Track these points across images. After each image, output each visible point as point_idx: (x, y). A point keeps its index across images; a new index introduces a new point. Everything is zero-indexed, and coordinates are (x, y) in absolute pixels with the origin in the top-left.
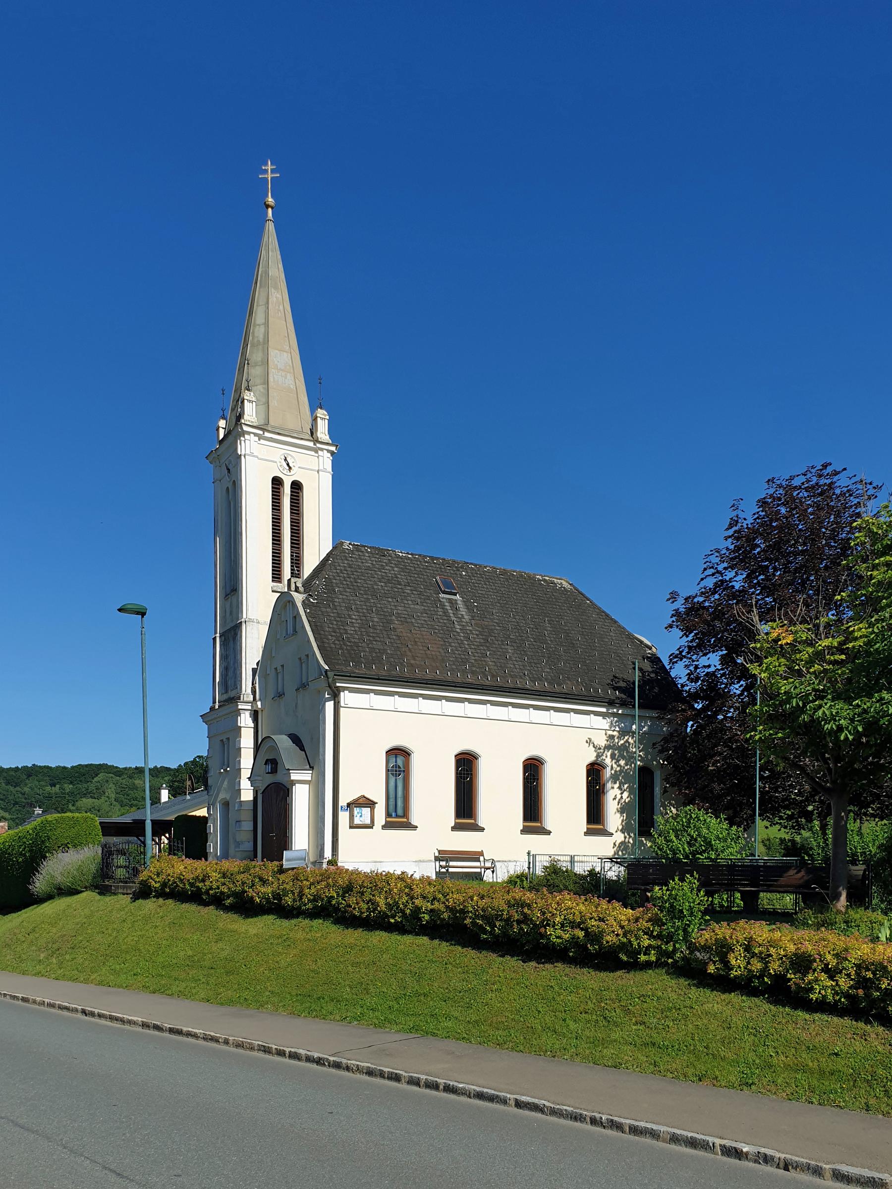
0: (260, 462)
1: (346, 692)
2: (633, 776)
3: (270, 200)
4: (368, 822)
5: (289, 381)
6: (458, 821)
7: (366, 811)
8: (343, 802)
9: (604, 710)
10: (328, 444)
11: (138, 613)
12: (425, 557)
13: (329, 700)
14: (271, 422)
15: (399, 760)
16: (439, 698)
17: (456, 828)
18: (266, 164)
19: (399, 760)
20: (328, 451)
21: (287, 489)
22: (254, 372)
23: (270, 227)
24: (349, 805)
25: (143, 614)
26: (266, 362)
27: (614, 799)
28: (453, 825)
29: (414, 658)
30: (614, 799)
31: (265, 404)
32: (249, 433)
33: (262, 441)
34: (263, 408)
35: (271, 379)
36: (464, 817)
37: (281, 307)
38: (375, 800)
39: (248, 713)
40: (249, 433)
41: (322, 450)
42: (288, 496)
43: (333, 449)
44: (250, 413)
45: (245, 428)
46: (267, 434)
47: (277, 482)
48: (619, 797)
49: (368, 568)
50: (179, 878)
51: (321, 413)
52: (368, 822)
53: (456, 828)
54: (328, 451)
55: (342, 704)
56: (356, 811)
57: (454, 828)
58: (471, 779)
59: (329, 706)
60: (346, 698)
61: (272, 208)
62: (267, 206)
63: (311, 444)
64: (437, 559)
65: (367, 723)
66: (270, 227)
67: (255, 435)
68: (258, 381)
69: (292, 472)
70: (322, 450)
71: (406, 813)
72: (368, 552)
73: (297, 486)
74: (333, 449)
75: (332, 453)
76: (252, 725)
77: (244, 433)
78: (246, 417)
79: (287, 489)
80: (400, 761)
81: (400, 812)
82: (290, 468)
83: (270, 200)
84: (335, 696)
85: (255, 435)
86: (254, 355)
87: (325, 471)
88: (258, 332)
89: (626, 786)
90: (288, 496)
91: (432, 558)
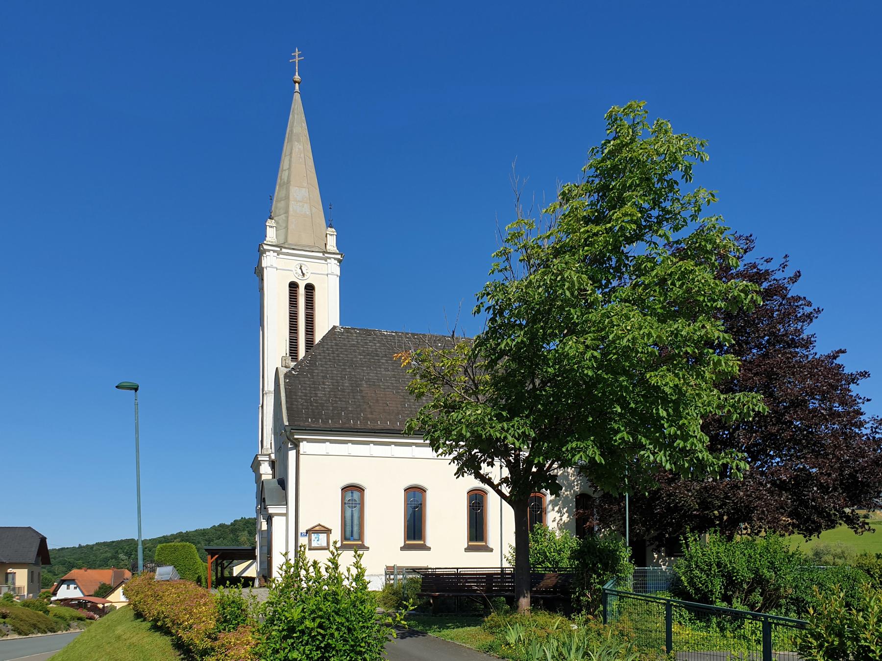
0: (278, 272)
1: (305, 442)
2: (571, 501)
3: (297, 77)
4: (325, 544)
5: (306, 209)
6: (140, 548)
7: (323, 536)
8: (302, 529)
9: (422, 441)
10: (334, 253)
11: (131, 389)
12: (407, 334)
13: (291, 449)
14: (290, 241)
15: (353, 495)
16: (410, 445)
17: (469, 549)
18: (295, 52)
19: (353, 495)
20: (335, 259)
21: (302, 291)
22: (277, 206)
23: (297, 97)
24: (307, 532)
25: (136, 390)
26: (287, 198)
27: (554, 521)
28: (402, 545)
29: (372, 413)
30: (554, 521)
31: (283, 229)
32: (269, 251)
33: (281, 256)
34: (282, 232)
35: (291, 209)
36: (476, 540)
37: (302, 155)
38: (330, 528)
39: (267, 464)
40: (269, 251)
41: (330, 258)
42: (302, 296)
43: (339, 257)
44: (271, 235)
45: (265, 247)
46: (284, 250)
47: (293, 286)
48: (558, 519)
49: (353, 345)
50: (860, 567)
51: (331, 231)
52: (325, 544)
53: (469, 549)
54: (335, 259)
55: (301, 452)
56: (313, 536)
57: (467, 550)
58: (482, 510)
59: (292, 454)
60: (304, 447)
61: (299, 83)
62: (295, 82)
63: (321, 255)
64: (417, 335)
65: (324, 466)
66: (297, 97)
67: (274, 251)
68: (282, 211)
69: (306, 277)
70: (330, 258)
71: (361, 537)
72: (356, 333)
73: (310, 288)
74: (339, 257)
75: (339, 261)
76: (271, 472)
77: (265, 251)
78: (267, 239)
79: (302, 291)
80: (356, 495)
81: (356, 536)
82: (303, 274)
83: (297, 77)
84: (296, 446)
85: (274, 251)
86: (279, 193)
87: (332, 274)
88: (283, 175)
89: (565, 510)
90: (302, 296)
91: (413, 335)
